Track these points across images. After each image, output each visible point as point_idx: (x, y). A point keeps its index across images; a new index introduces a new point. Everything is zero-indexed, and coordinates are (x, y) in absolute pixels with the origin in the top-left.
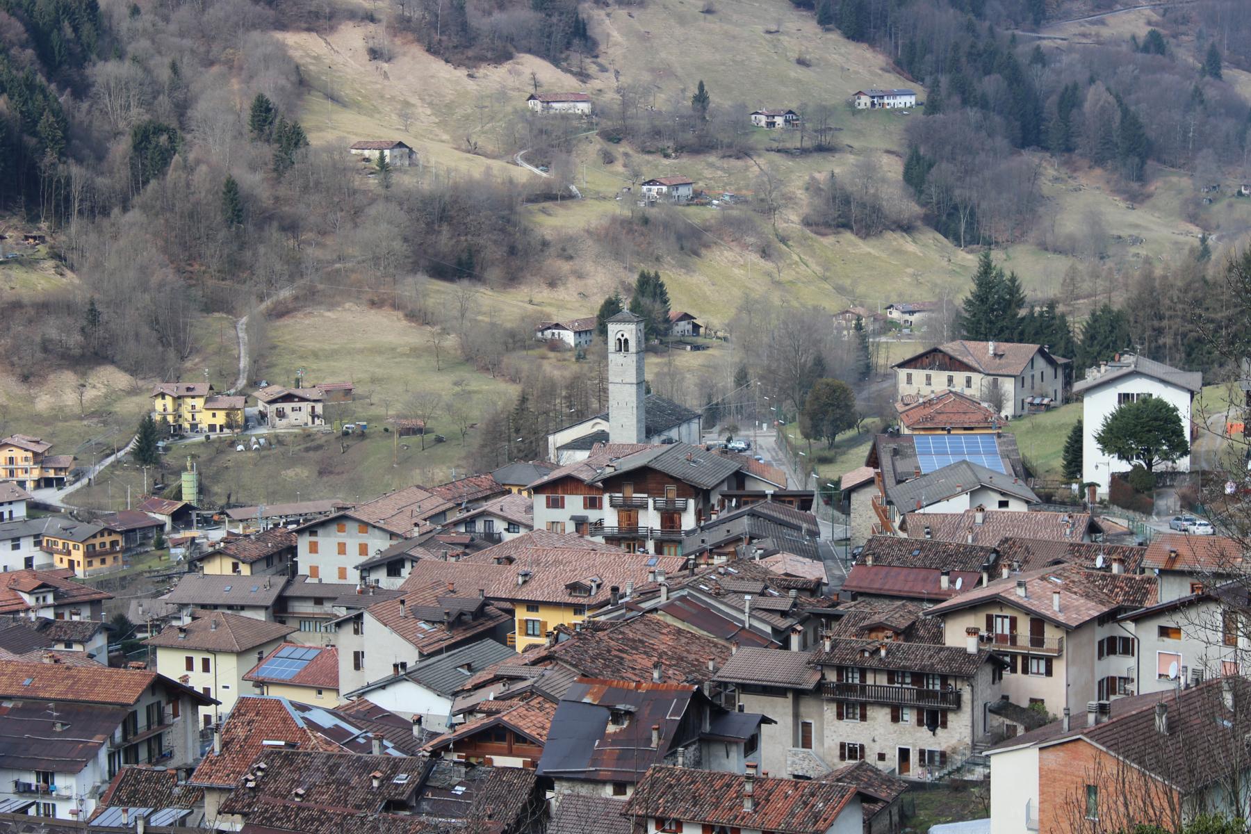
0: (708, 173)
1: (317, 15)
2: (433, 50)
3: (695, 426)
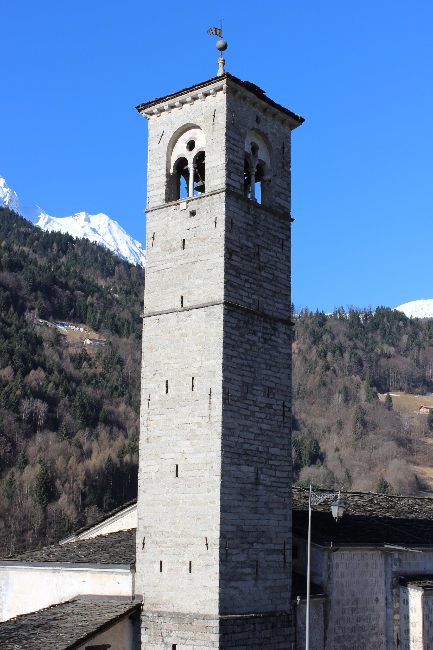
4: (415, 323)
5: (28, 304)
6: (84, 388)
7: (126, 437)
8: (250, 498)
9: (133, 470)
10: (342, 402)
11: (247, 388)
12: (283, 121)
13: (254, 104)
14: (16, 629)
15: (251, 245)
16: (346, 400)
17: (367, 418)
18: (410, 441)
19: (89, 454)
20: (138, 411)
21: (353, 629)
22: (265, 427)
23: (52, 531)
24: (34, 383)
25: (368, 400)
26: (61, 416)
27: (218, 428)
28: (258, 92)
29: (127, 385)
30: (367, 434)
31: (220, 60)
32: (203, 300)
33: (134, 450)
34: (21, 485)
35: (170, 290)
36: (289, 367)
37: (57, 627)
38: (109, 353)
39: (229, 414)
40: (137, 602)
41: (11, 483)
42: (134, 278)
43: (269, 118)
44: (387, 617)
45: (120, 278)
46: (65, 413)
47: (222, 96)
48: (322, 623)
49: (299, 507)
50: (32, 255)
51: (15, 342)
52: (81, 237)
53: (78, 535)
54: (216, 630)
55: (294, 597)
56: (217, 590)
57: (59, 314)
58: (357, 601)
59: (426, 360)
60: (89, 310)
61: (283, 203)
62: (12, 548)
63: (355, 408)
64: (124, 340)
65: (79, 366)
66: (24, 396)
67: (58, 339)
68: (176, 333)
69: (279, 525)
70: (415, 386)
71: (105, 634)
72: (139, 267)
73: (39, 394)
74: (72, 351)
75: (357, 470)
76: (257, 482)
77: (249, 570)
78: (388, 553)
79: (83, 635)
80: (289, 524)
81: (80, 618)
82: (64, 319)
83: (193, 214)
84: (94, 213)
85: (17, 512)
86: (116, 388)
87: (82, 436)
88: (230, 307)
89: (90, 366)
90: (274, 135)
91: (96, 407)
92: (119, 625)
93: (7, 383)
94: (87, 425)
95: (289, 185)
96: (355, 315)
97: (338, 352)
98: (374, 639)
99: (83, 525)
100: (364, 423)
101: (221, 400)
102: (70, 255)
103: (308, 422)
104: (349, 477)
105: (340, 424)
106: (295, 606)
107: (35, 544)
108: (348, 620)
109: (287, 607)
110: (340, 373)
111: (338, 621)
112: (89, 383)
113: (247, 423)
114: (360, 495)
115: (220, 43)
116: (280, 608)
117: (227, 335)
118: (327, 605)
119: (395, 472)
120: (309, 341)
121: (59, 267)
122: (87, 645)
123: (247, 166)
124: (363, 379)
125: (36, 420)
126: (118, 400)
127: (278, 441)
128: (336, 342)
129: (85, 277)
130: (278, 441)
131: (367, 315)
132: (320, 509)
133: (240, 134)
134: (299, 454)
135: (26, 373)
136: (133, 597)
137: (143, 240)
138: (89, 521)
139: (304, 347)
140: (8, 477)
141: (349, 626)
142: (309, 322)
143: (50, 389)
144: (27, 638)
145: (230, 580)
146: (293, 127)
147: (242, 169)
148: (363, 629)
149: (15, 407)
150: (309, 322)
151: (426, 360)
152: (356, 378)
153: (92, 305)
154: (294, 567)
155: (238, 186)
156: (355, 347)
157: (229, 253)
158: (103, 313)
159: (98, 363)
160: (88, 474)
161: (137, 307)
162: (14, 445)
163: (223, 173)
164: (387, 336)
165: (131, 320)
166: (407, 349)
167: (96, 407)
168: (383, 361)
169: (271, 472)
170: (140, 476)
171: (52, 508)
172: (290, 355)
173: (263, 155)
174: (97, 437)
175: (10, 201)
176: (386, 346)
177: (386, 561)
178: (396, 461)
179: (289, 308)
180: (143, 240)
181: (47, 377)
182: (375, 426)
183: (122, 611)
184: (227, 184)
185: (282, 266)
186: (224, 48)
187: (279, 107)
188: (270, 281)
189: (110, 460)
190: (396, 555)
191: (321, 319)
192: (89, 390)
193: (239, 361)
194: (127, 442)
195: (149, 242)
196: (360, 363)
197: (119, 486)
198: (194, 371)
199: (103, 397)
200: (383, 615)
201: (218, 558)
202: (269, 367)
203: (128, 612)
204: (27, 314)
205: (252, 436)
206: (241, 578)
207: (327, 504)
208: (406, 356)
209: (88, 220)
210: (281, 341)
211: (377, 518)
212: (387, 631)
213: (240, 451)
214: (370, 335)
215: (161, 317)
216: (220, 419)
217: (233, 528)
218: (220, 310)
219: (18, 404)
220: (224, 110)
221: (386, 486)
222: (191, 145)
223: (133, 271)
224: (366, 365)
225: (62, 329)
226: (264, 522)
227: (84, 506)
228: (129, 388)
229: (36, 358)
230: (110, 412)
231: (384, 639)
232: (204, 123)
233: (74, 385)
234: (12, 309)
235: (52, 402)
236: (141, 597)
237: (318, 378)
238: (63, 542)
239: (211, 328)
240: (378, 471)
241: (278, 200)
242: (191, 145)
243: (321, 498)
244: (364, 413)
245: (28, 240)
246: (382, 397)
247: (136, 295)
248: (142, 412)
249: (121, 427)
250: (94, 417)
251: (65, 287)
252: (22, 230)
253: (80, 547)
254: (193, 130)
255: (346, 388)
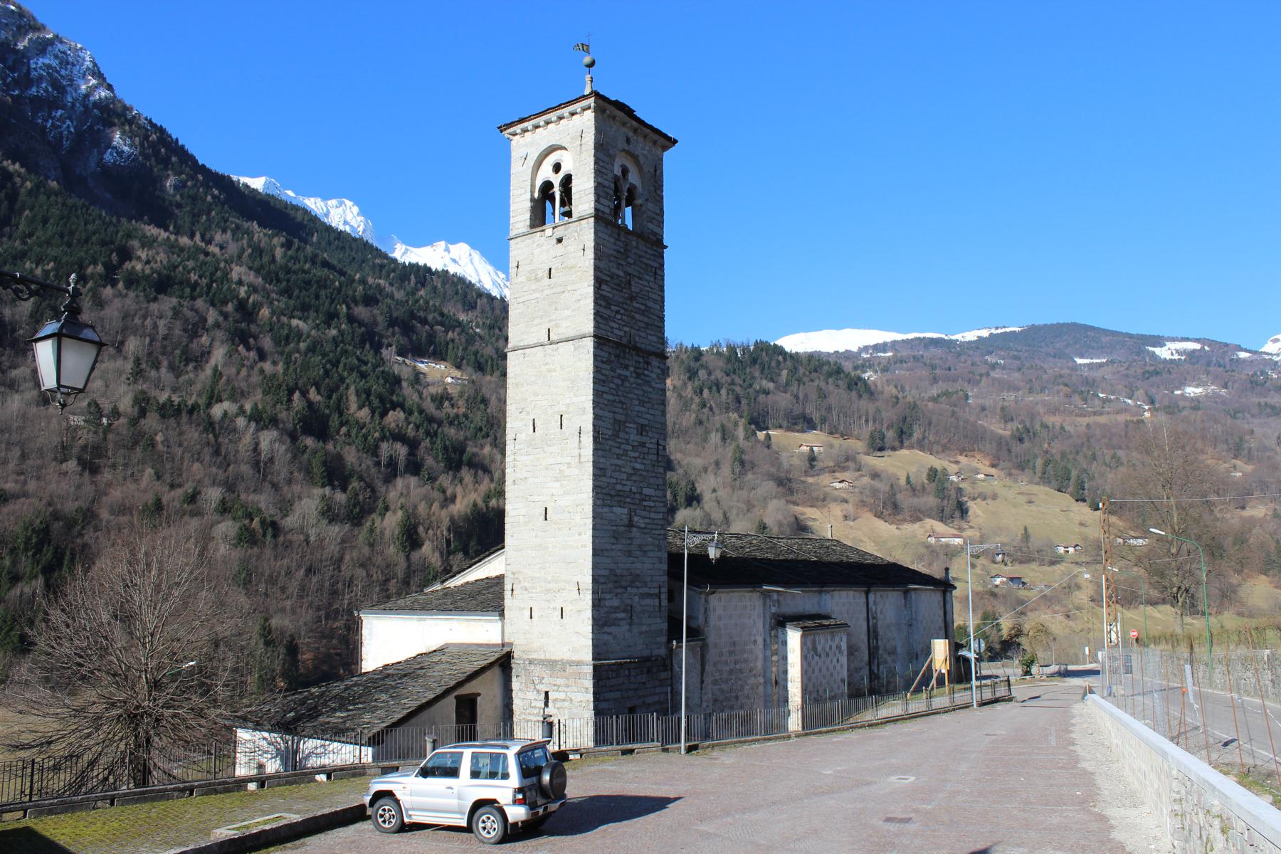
0: (1031, 574)
1: (817, 499)
2: (879, 515)
3: (837, 510)
4: (795, 358)
5: (385, 341)
6: (446, 429)
7: (492, 480)
8: (623, 541)
9: (500, 514)
10: (719, 441)
11: (619, 426)
12: (655, 143)
13: (624, 124)
14: (383, 679)
15: (621, 274)
16: (724, 439)
17: (745, 457)
18: (790, 480)
19: (453, 499)
20: (503, 453)
21: (731, 672)
22: (638, 466)
23: (416, 580)
24: (393, 425)
25: (746, 438)
26: (422, 459)
27: (589, 468)
28: (629, 112)
29: (492, 425)
30: (745, 473)
31: (588, 78)
32: (571, 333)
33: (501, 494)
34: (382, 532)
35: (536, 322)
36: (663, 403)
37: (424, 676)
38: (472, 392)
39: (600, 453)
40: (506, 649)
41: (372, 530)
42: (497, 312)
43: (641, 139)
44: (765, 659)
45: (483, 312)
46: (426, 456)
47: (590, 115)
48: (699, 667)
49: (674, 550)
50: (388, 289)
51: (372, 382)
52: (440, 269)
53: (443, 582)
54: (590, 677)
55: (670, 641)
56: (590, 636)
57: (418, 351)
58: (734, 644)
59: (806, 396)
60: (450, 346)
61: (656, 230)
62: (375, 597)
63: (733, 446)
64: (488, 378)
65: (440, 406)
66: (383, 438)
67: (417, 377)
68: (543, 368)
69: (654, 567)
70: (795, 424)
71: (474, 682)
72: (502, 299)
73: (399, 437)
74: (433, 390)
75: (734, 511)
76: (630, 525)
77: (623, 615)
78: (766, 595)
79: (452, 683)
80: (665, 567)
81: (448, 666)
82: (423, 357)
83: (560, 241)
84: (454, 242)
85: (379, 560)
86: (481, 429)
87: (445, 480)
88: (601, 341)
89: (453, 406)
90: (646, 157)
91: (460, 449)
92: (488, 674)
93: (365, 425)
94: (450, 469)
95: (662, 210)
96: (732, 349)
97: (714, 388)
98: (752, 681)
99: (449, 572)
100: (742, 463)
101: (591, 439)
102: (428, 288)
103: (684, 463)
104: (726, 518)
105: (717, 464)
106: (671, 650)
107: (399, 594)
108: (726, 663)
109: (663, 652)
110: (716, 410)
111: (715, 664)
112: (451, 424)
113: (619, 462)
114: (738, 536)
115: (587, 60)
116: (656, 652)
117: (597, 370)
118: (704, 648)
119: (775, 513)
120: (684, 377)
121: (417, 301)
122: (456, 693)
123: (617, 190)
124: (741, 417)
125: (396, 464)
126: (483, 441)
127: (652, 481)
128: (713, 377)
129: (446, 311)
130: (652, 481)
131: (745, 349)
132: (696, 551)
133: (609, 156)
134: (675, 496)
135: (384, 414)
136: (503, 645)
137: (505, 270)
138: (455, 569)
139: (678, 383)
140: (368, 524)
141: (727, 669)
142: (684, 357)
143: (410, 431)
144: (393, 687)
145: (604, 625)
146: (665, 148)
147: (612, 193)
148: (741, 671)
149: (374, 451)
150: (684, 357)
151: (806, 396)
152: (734, 416)
153: (453, 340)
154: (670, 611)
155: (607, 210)
156: (733, 383)
157: (599, 283)
158: (465, 349)
159: (460, 403)
160: (452, 520)
161: (501, 342)
162: (373, 491)
163: (592, 197)
164: (766, 371)
165: (495, 356)
166: (787, 384)
167: (460, 449)
168: (762, 398)
169: (645, 513)
170: (507, 520)
171: (415, 556)
172: (664, 390)
173: (633, 178)
174: (461, 481)
175: (365, 230)
176: (764, 382)
177: (764, 604)
178: (775, 502)
179: (663, 341)
180: (505, 270)
181: (406, 419)
182: (753, 466)
183: (492, 659)
184: (596, 209)
185: (655, 297)
186: (592, 65)
187: (651, 127)
188: (642, 313)
189: (475, 505)
190: (775, 596)
191: (697, 354)
192: (452, 431)
193: (611, 397)
194: (492, 486)
195: (513, 271)
196: (738, 400)
197: (485, 532)
198: (562, 409)
199: (466, 439)
200: (761, 656)
201: (590, 603)
202: (642, 403)
203: (498, 660)
204: (384, 352)
205: (625, 476)
206: (615, 623)
207: (703, 546)
208: (785, 392)
209: (447, 250)
210: (654, 376)
211: (755, 559)
212: (765, 672)
213: (613, 493)
214: (748, 370)
215: (527, 351)
216: (591, 459)
217: (607, 573)
218: (589, 344)
219: (377, 447)
220: (592, 131)
221: (765, 528)
222: (557, 168)
223: (496, 304)
224: (744, 402)
225: (422, 367)
226: (638, 565)
227: (449, 553)
228: (494, 429)
229: (394, 398)
230: (475, 455)
231: (762, 680)
232: (572, 143)
233: (435, 426)
234: (368, 346)
235: (413, 445)
236: (511, 644)
237: (694, 416)
238: (428, 590)
239: (579, 363)
240: (757, 512)
241: (651, 226)
242: (557, 168)
243: (698, 539)
244: (743, 452)
245: (384, 272)
246: (761, 435)
247: (500, 330)
248: (508, 453)
249: (486, 470)
250: (457, 460)
251: (424, 321)
252: (378, 261)
253: (446, 595)
254: (559, 152)
255: (723, 426)
